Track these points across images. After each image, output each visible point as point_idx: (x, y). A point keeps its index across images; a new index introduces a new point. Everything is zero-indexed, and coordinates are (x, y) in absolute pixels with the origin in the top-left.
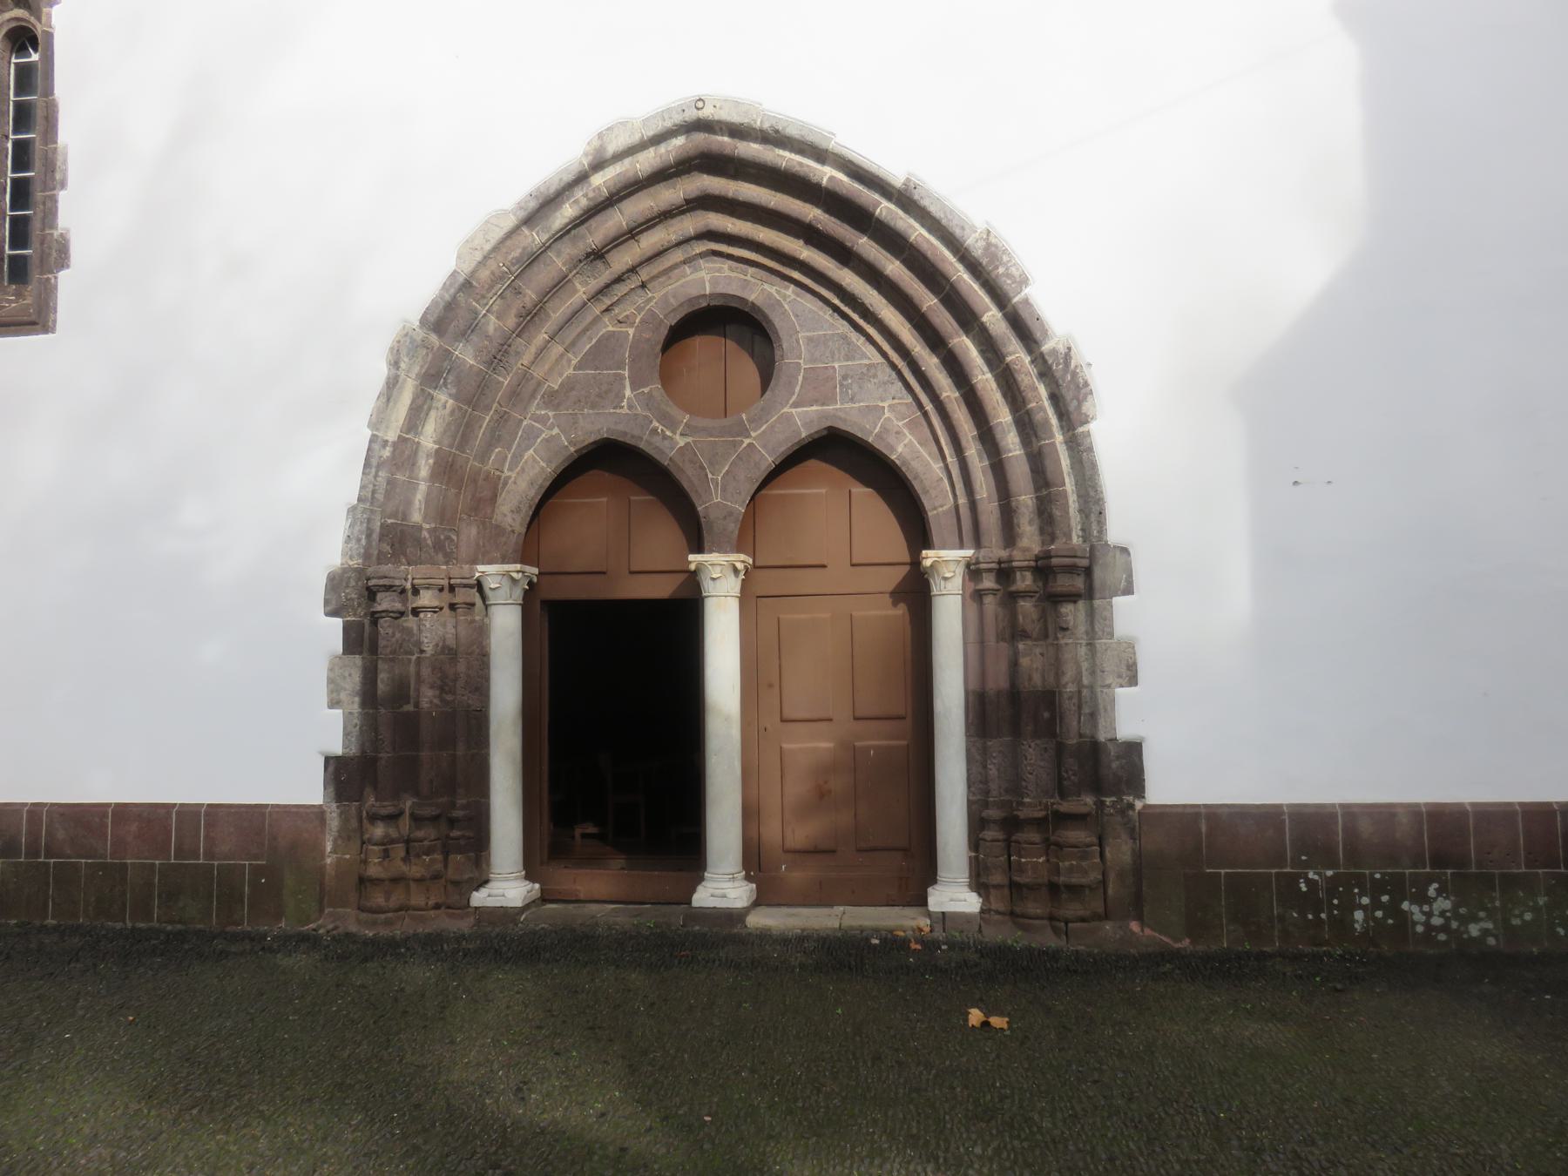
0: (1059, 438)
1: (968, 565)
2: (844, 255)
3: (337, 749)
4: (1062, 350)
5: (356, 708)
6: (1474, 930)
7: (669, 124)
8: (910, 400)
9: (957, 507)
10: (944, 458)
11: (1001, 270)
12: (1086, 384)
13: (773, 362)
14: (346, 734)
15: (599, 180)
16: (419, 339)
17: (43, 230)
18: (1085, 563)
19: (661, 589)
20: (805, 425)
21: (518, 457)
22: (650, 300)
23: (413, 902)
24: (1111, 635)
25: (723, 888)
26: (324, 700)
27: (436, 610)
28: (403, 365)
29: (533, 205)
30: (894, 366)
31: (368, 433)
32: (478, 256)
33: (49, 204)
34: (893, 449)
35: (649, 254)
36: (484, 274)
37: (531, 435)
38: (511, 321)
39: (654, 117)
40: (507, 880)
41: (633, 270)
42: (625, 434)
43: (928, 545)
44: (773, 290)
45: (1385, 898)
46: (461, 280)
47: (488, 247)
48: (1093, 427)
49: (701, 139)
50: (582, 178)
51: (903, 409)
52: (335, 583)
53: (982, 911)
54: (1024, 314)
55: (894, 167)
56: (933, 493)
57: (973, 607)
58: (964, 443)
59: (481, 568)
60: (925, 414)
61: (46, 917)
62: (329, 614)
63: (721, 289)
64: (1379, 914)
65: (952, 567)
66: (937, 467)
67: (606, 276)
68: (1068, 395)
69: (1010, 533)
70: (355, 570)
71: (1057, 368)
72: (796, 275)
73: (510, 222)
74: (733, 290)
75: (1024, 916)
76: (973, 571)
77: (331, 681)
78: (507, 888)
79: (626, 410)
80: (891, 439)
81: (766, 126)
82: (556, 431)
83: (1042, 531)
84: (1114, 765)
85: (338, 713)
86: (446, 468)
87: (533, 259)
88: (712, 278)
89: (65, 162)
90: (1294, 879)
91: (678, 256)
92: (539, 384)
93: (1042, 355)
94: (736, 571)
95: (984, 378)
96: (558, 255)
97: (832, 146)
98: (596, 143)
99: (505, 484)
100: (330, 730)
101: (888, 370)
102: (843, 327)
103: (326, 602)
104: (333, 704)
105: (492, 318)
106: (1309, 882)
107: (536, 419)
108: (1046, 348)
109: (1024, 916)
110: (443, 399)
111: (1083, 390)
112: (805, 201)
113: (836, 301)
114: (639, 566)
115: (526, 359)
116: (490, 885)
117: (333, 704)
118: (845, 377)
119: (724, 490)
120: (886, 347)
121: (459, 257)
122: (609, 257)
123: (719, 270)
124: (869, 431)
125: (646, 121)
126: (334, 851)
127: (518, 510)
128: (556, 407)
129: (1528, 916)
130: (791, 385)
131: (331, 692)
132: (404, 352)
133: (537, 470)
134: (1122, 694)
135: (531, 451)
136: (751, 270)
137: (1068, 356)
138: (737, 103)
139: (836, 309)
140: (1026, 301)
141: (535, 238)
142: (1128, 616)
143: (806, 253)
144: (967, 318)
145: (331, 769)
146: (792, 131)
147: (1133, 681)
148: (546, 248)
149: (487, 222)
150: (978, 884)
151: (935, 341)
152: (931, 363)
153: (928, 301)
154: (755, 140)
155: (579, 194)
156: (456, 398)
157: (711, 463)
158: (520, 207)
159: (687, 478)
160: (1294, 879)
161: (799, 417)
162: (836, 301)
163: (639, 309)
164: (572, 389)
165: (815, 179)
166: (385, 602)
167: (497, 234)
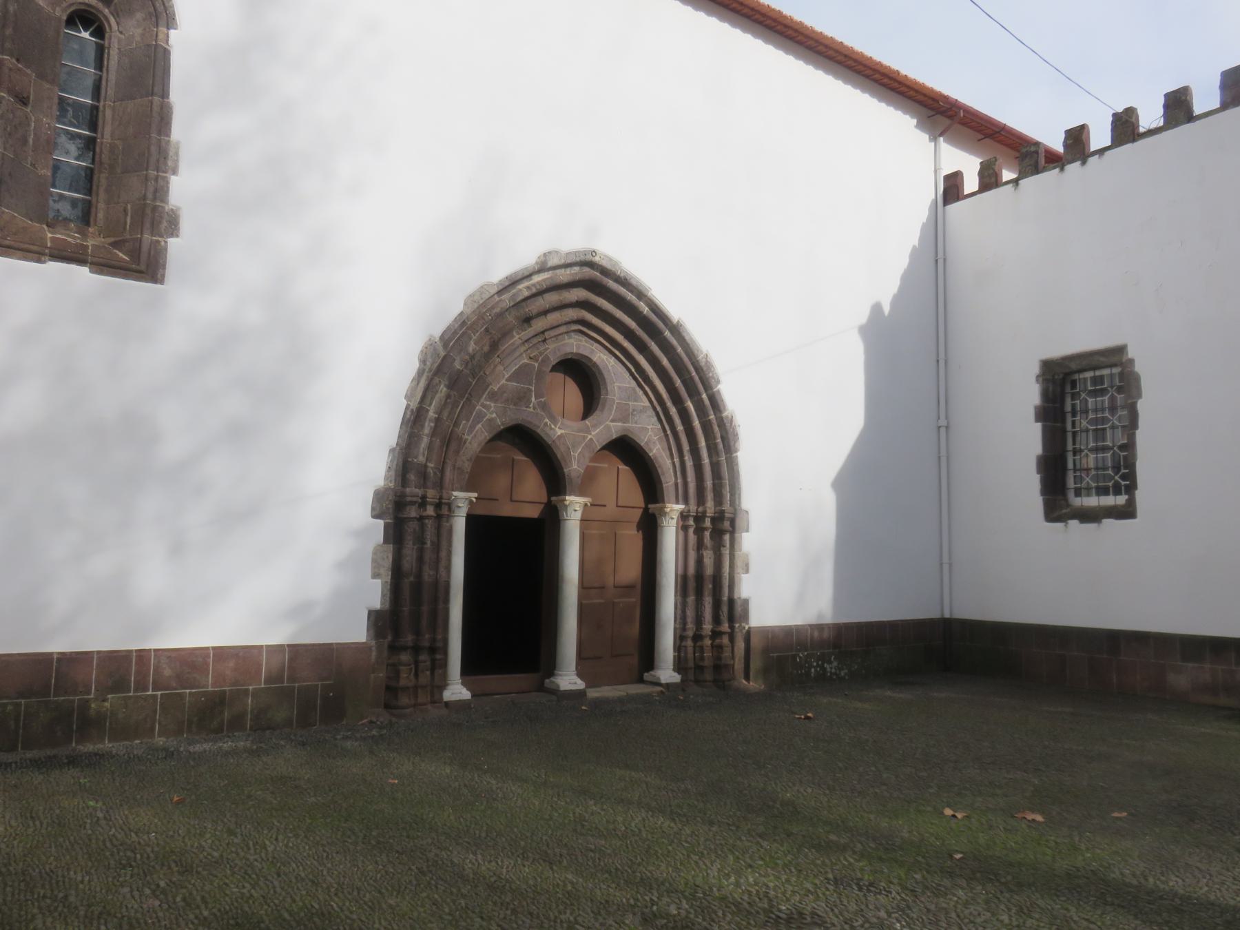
2: (642, 348)
14: (383, 596)
15: (537, 279)
17: (155, 199)
19: (533, 512)
21: (472, 427)
25: (568, 679)
26: (370, 574)
30: (654, 409)
31: (405, 403)
33: (161, 182)
38: (486, 349)
48: (739, 454)
49: (588, 272)
50: (529, 276)
52: (379, 496)
57: (681, 533)
59: (455, 493)
60: (666, 436)
61: (152, 736)
62: (375, 516)
63: (581, 351)
66: (669, 462)
69: (701, 500)
72: (617, 353)
76: (683, 516)
77: (374, 561)
78: (457, 691)
85: (378, 582)
88: (577, 345)
89: (177, 154)
90: (794, 657)
91: (563, 329)
100: (374, 594)
102: (634, 384)
103: (373, 509)
107: (484, 406)
108: (724, 415)
110: (443, 390)
114: (524, 496)
121: (465, 304)
122: (533, 322)
128: (496, 402)
131: (373, 568)
134: (744, 576)
138: (610, 259)
143: (626, 344)
145: (372, 618)
147: (747, 571)
150: (580, 674)
151: (677, 401)
152: (673, 411)
159: (560, 451)
160: (794, 657)
161: (604, 427)
163: (541, 354)
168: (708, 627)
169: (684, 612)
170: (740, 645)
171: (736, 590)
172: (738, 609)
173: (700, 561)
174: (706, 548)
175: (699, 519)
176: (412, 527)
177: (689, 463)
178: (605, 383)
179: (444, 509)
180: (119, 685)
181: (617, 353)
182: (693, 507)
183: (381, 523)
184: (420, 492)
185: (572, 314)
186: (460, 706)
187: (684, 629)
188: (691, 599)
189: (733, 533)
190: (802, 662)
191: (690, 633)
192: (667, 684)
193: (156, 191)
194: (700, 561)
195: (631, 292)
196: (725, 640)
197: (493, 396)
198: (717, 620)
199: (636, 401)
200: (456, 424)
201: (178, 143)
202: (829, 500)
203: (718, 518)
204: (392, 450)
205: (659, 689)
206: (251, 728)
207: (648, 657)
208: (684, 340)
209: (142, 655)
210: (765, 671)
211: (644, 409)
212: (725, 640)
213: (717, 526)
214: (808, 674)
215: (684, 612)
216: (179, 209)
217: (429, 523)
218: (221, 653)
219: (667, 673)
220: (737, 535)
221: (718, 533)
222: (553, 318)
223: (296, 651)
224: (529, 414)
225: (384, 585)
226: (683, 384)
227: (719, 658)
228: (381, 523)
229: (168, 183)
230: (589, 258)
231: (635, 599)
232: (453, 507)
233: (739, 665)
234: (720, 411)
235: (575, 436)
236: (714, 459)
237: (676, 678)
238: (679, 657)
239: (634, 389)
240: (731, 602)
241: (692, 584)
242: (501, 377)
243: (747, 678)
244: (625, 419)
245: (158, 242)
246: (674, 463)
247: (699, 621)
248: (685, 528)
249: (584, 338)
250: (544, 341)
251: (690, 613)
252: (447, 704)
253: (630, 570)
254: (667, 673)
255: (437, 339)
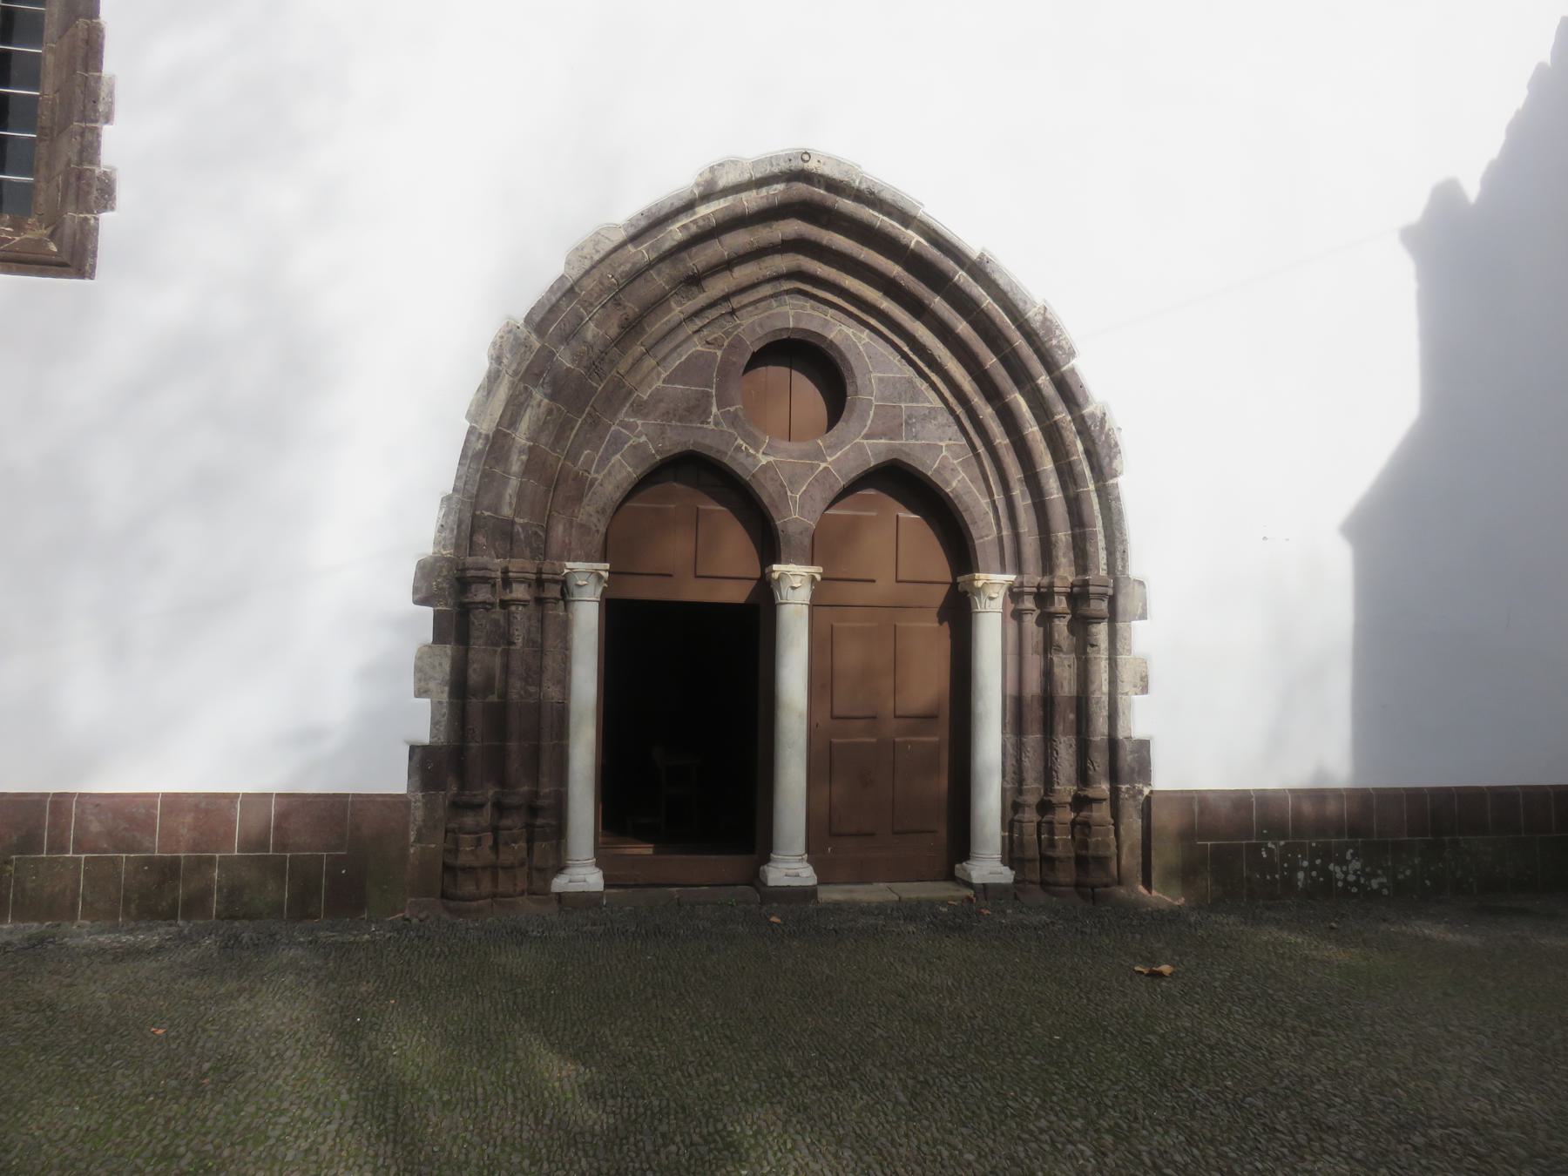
0: (1092, 487)
1: (1010, 589)
2: (918, 309)
3: (424, 736)
4: (1099, 414)
5: (445, 697)
6: (1375, 884)
7: (776, 170)
8: (964, 441)
9: (1000, 539)
10: (991, 494)
11: (1054, 342)
12: (1116, 445)
13: (844, 395)
14: (434, 723)
15: (703, 210)
16: (522, 337)
17: (80, 162)
18: (1110, 592)
19: (736, 594)
20: (875, 455)
21: (604, 460)
22: (738, 326)
23: (501, 889)
24: (1129, 651)
25: (790, 868)
27: (524, 603)
28: (505, 361)
29: (643, 223)
30: (952, 412)
31: (466, 424)
32: (587, 264)
33: (89, 136)
34: (948, 483)
35: (745, 284)
36: (590, 283)
37: (617, 442)
38: (614, 331)
39: (762, 161)
40: (584, 866)
41: (726, 298)
42: (711, 448)
43: (777, 559)
44: (850, 332)
45: (1318, 862)
46: (568, 285)
47: (597, 257)
49: (801, 189)
50: (689, 206)
51: (958, 450)
52: (426, 570)
53: (1016, 881)
54: (1071, 381)
55: (972, 241)
56: (981, 524)
57: (1012, 624)
58: (1012, 484)
59: (569, 565)
60: (977, 456)
63: (803, 325)
64: (1314, 874)
65: (997, 588)
66: (984, 502)
67: (701, 299)
68: (1103, 452)
70: (448, 560)
71: (1095, 429)
72: (873, 322)
73: (620, 236)
74: (814, 326)
75: (1056, 884)
76: (1014, 594)
77: (418, 670)
79: (712, 426)
80: (947, 475)
81: (863, 186)
82: (643, 439)
83: (1076, 564)
84: (1129, 758)
85: (426, 703)
86: (535, 463)
87: (638, 274)
88: (797, 314)
89: (111, 93)
90: (1256, 849)
91: (766, 290)
92: (630, 393)
93: (1082, 417)
94: (600, 577)
95: (1033, 431)
96: (658, 274)
97: (920, 214)
98: (708, 176)
99: (592, 485)
100: (419, 721)
101: (947, 414)
102: (909, 372)
103: (416, 590)
104: (420, 693)
105: (592, 325)
106: (1269, 851)
108: (1086, 411)
109: (1056, 884)
111: (1113, 449)
112: (888, 257)
113: (906, 349)
114: (714, 570)
115: (623, 368)
116: (568, 871)
117: (420, 693)
118: (910, 417)
119: (802, 507)
120: (947, 394)
121: (568, 263)
122: (705, 283)
123: (803, 307)
124: (930, 467)
125: (755, 164)
126: (419, 839)
127: (604, 511)
128: (645, 416)
129: (1408, 873)
130: (863, 419)
131: (418, 680)
132: (506, 348)
133: (624, 474)
135: (618, 456)
136: (831, 311)
137: (1103, 421)
138: (839, 163)
139: (904, 356)
140: (1073, 370)
141: (643, 253)
142: (1143, 638)
143: (886, 304)
144: (1022, 377)
145: (417, 758)
146: (887, 196)
148: (651, 265)
149: (597, 233)
151: (993, 394)
152: (986, 412)
153: (991, 361)
154: (848, 197)
155: (685, 220)
156: (552, 397)
157: (791, 483)
158: (631, 223)
159: (766, 492)
160: (1256, 849)
161: (858, 446)
162: (906, 349)
163: (727, 334)
164: (661, 401)
165: (904, 241)
166: (482, 594)
167: (608, 246)
168: (1065, 788)
169: (1019, 761)
170: (1133, 823)
171: (1121, 723)
172: (1127, 758)
173: (1048, 674)
174: (1059, 649)
175: (1043, 597)
176: (479, 619)
177: (1023, 501)
178: (853, 375)
179: (552, 594)
180: (30, 843)
181: (873, 322)
182: (1033, 577)
183: (428, 612)
184: (498, 563)
185: (781, 263)
186: (586, 900)
187: (1020, 791)
188: (1033, 739)
189: (1113, 617)
190: (1257, 855)
191: (1032, 799)
192: (985, 887)
193: (81, 152)
194: (1048, 674)
195: (889, 215)
196: (1102, 813)
197: (640, 409)
198: (1083, 777)
199: (913, 400)
200: (573, 456)
201: (112, 78)
202: (1338, 564)
203: (1079, 595)
204: (447, 500)
205: (970, 893)
206: (218, 916)
207: (961, 843)
208: (997, 286)
209: (60, 802)
210: (1187, 874)
211: (931, 414)
212: (1102, 813)
213: (1081, 609)
214: (1289, 882)
215: (1019, 761)
216: (114, 170)
217: (518, 611)
218: (173, 802)
219: (988, 866)
220: (1120, 625)
221: (1081, 624)
222: (743, 274)
223: (295, 806)
224: (712, 433)
225: (436, 707)
226: (1000, 357)
227: (1084, 845)
228: (428, 612)
229: (99, 135)
230: (797, 164)
231: (938, 736)
232: (571, 585)
233: (1130, 860)
234: (1078, 406)
235: (799, 462)
236: (1071, 493)
237: (1006, 875)
238: (1011, 837)
239: (910, 381)
240: (1113, 744)
241: (1034, 714)
242: (657, 380)
243: (1147, 883)
244: (893, 433)
245: (86, 220)
246: (993, 502)
247: (1048, 775)
248: (1018, 615)
249: (809, 303)
250: (733, 312)
251: (1032, 763)
252: (560, 896)
253: (926, 684)
254: (988, 866)
255: (521, 322)
